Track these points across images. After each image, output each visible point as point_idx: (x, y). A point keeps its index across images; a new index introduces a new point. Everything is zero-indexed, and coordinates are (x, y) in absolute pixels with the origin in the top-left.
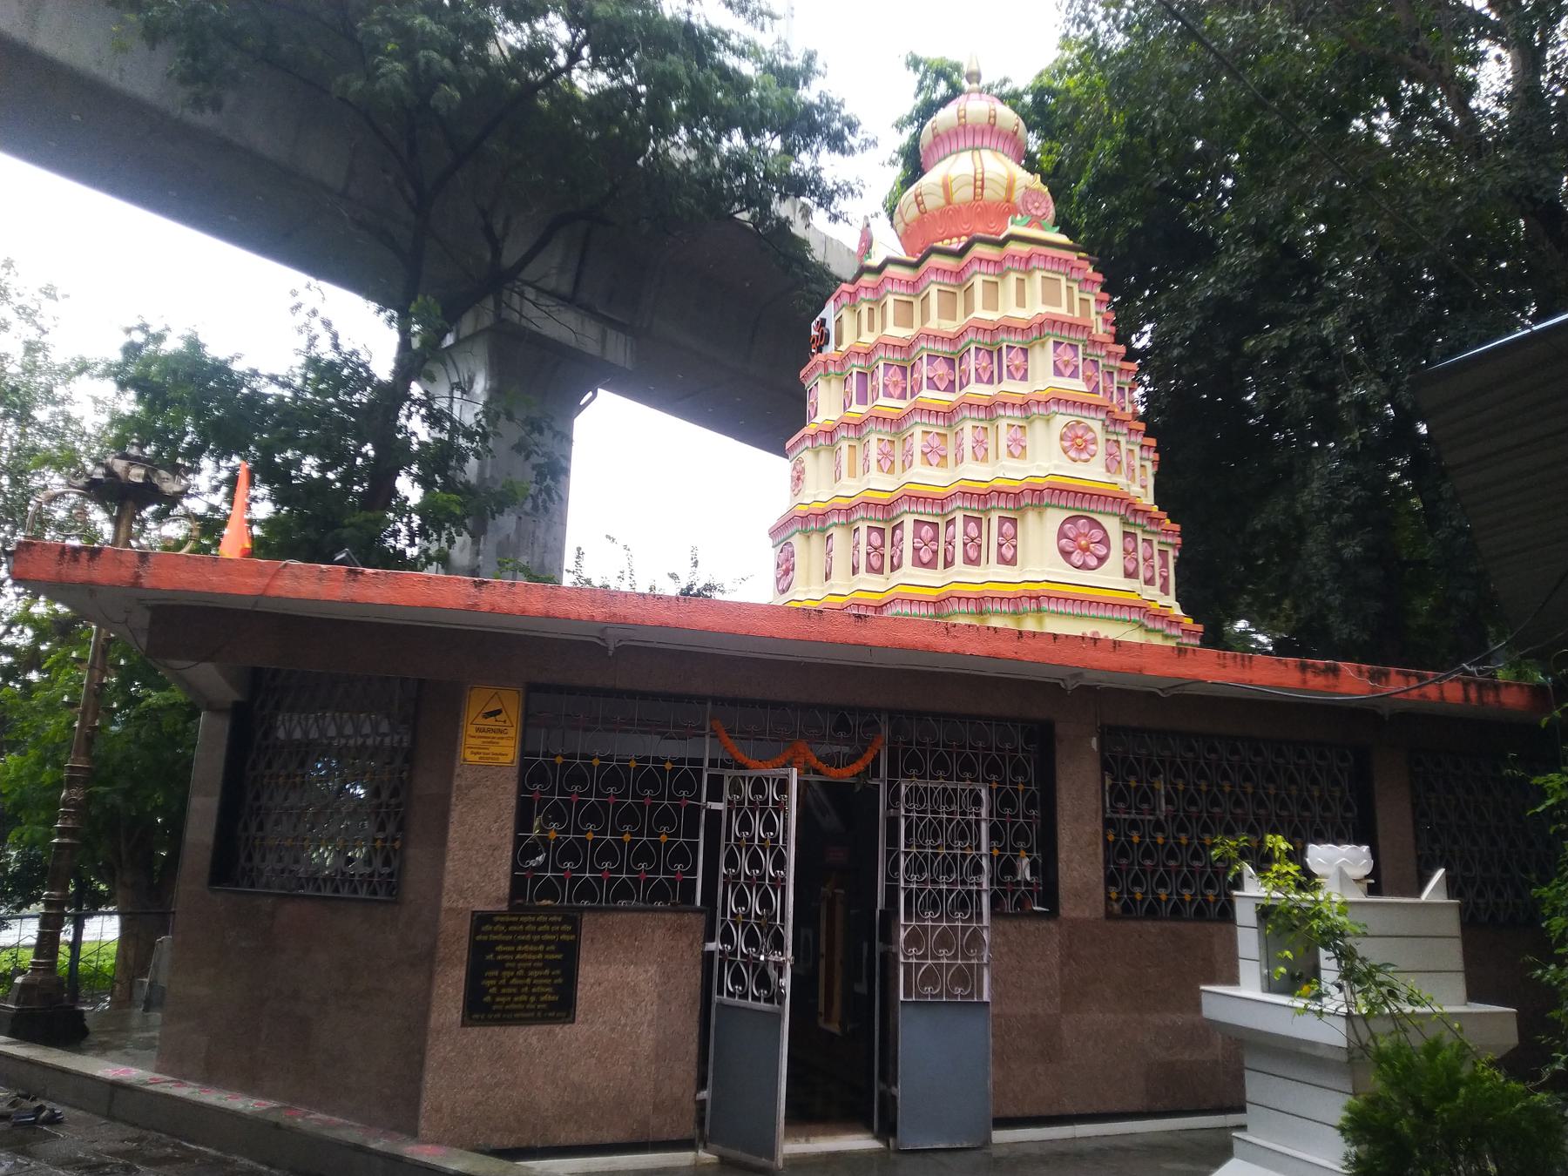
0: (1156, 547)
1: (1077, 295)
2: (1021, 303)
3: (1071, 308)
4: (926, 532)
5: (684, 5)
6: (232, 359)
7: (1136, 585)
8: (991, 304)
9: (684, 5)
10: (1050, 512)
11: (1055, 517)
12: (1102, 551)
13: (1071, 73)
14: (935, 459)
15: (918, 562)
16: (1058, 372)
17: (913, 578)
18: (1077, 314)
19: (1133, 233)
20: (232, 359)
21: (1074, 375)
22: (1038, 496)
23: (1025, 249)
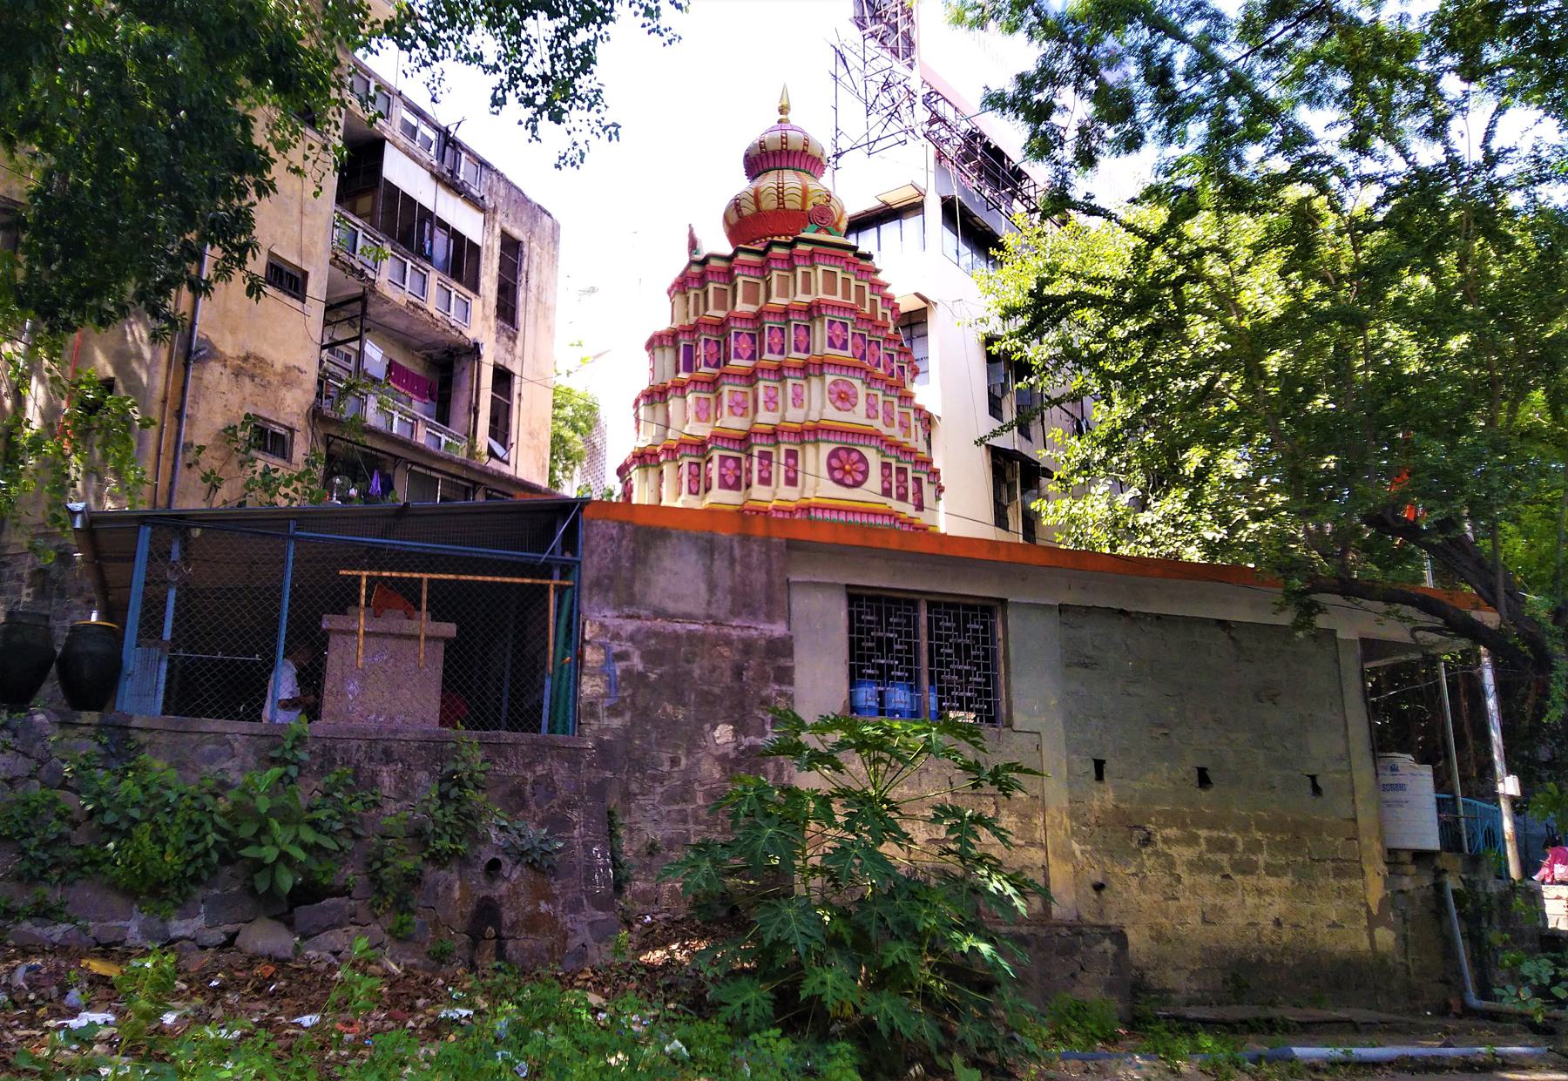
0: (910, 475)
1: (853, 283)
2: (807, 290)
3: (846, 295)
4: (730, 464)
5: (1354, 5)
6: (693, 245)
7: (894, 504)
8: (784, 293)
9: (1354, 5)
10: (822, 445)
11: (826, 449)
12: (862, 467)
13: (1121, 431)
14: (740, 411)
15: (724, 485)
16: (832, 344)
17: (719, 497)
18: (853, 301)
19: (1143, 1058)
20: (693, 245)
21: (844, 347)
22: (811, 433)
23: (809, 248)
